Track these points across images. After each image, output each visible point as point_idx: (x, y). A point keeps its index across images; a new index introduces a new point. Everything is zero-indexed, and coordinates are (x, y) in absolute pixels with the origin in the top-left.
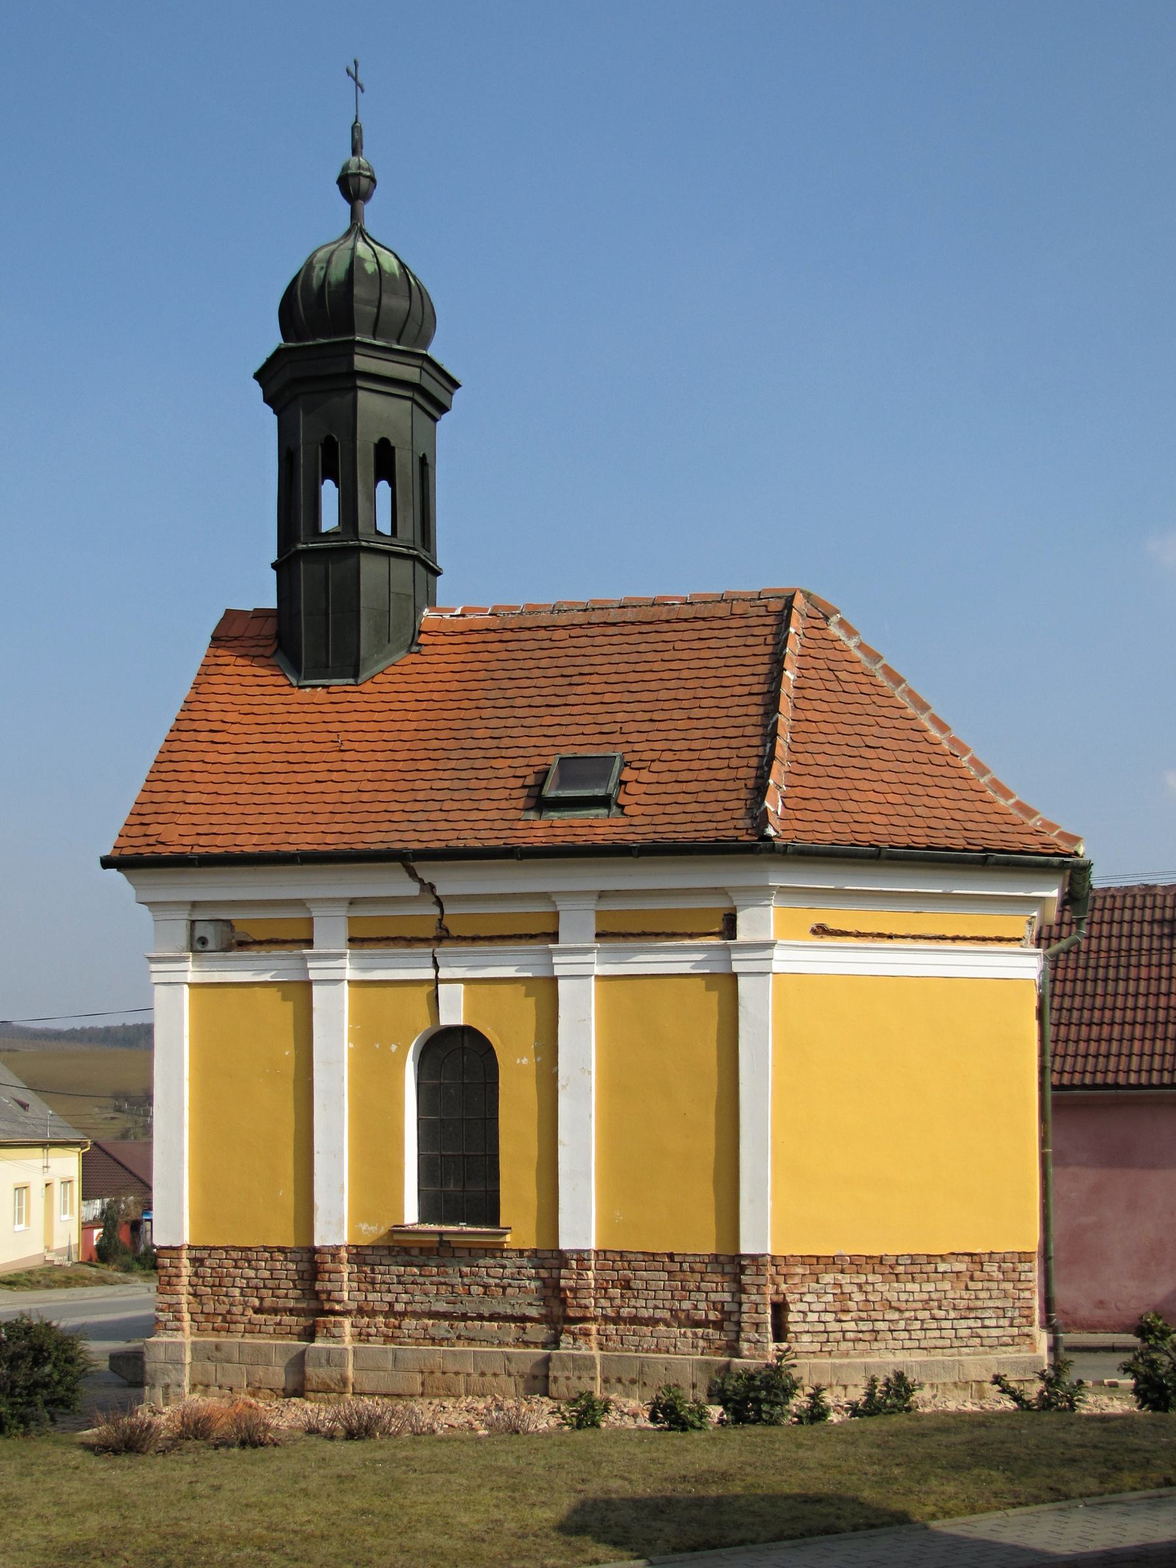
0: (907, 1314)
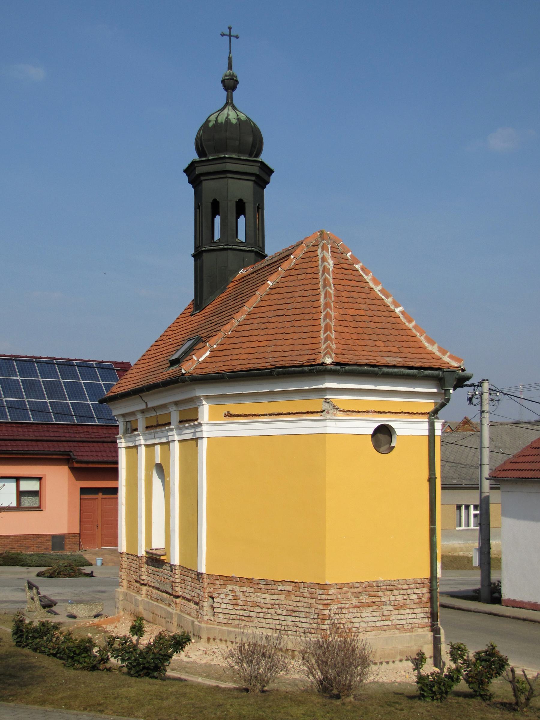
0: (264, 610)
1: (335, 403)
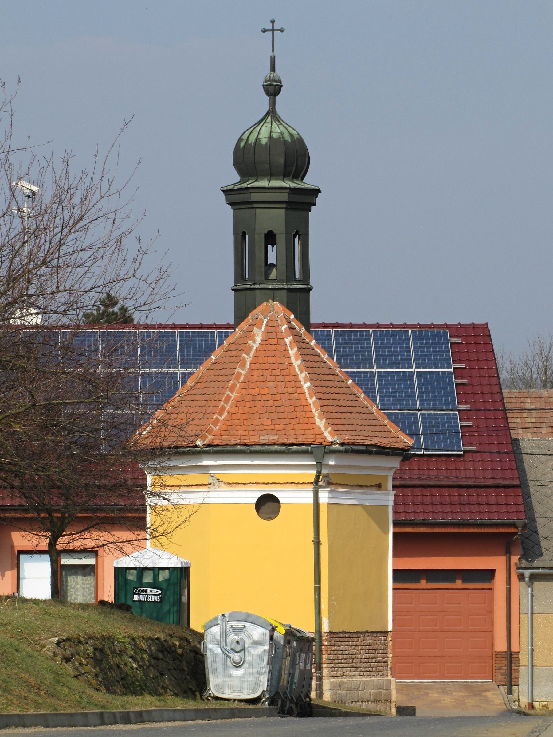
1: (216, 475)
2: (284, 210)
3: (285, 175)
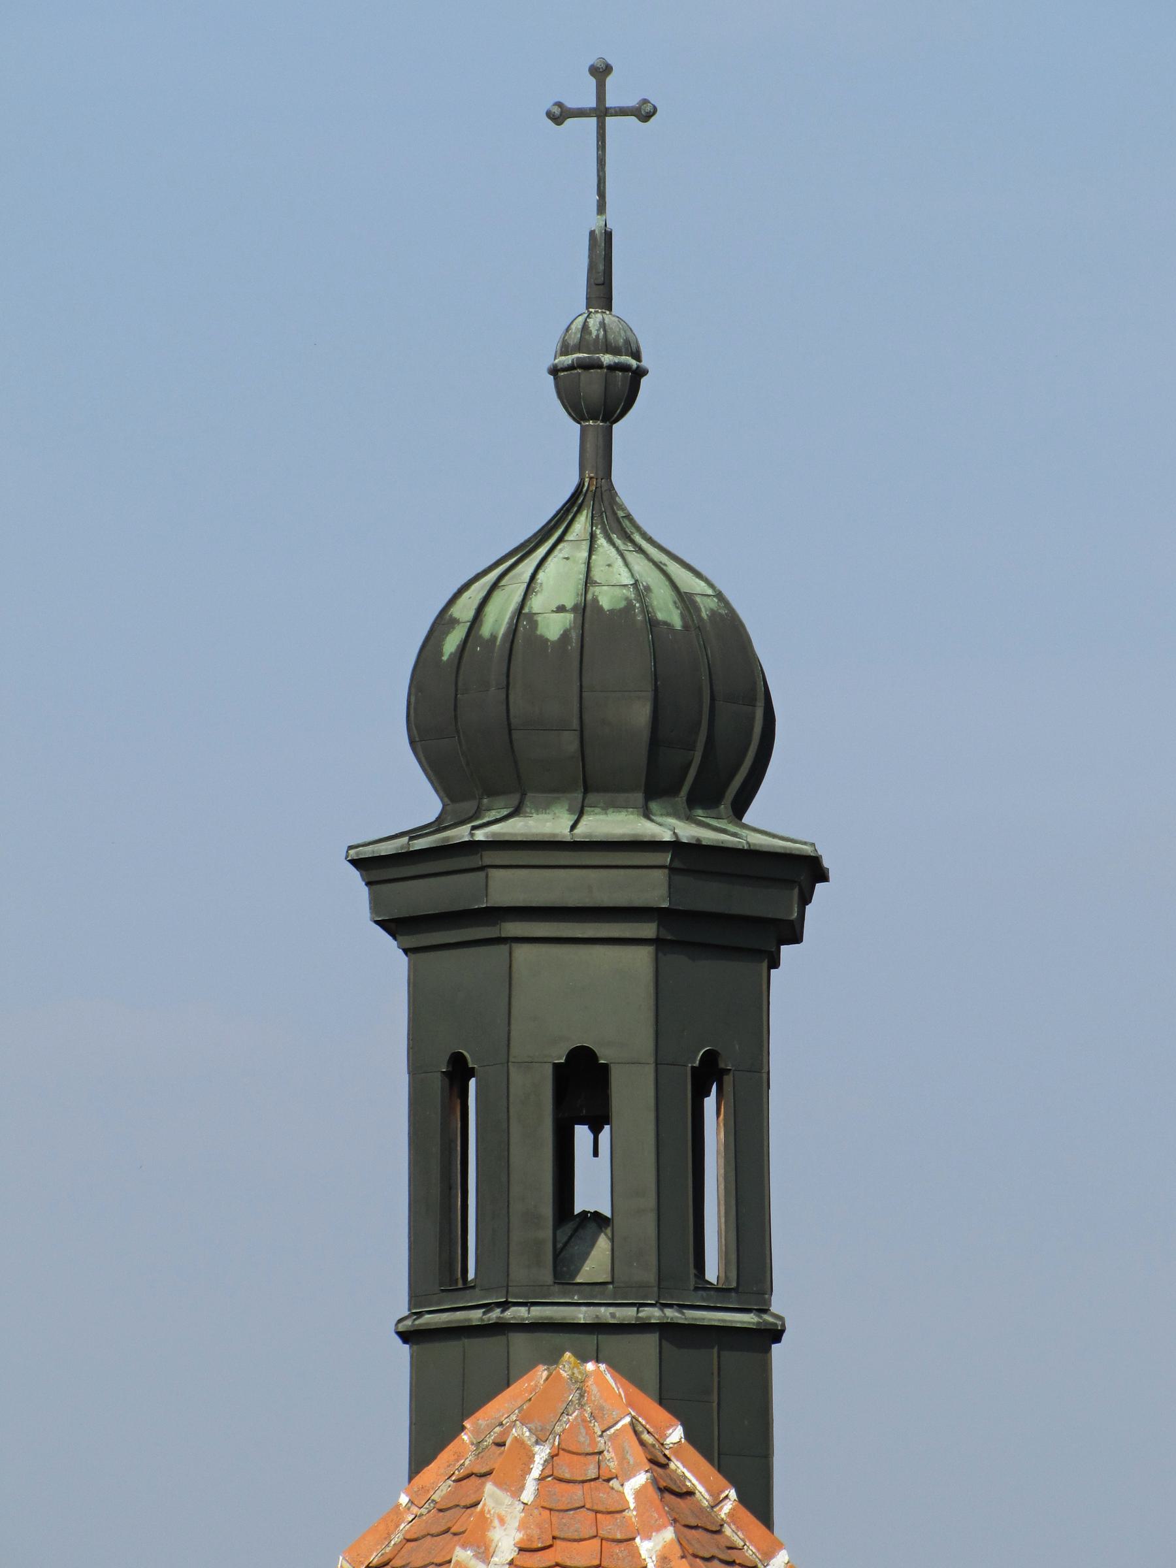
2: (642, 957)
3: (655, 789)
